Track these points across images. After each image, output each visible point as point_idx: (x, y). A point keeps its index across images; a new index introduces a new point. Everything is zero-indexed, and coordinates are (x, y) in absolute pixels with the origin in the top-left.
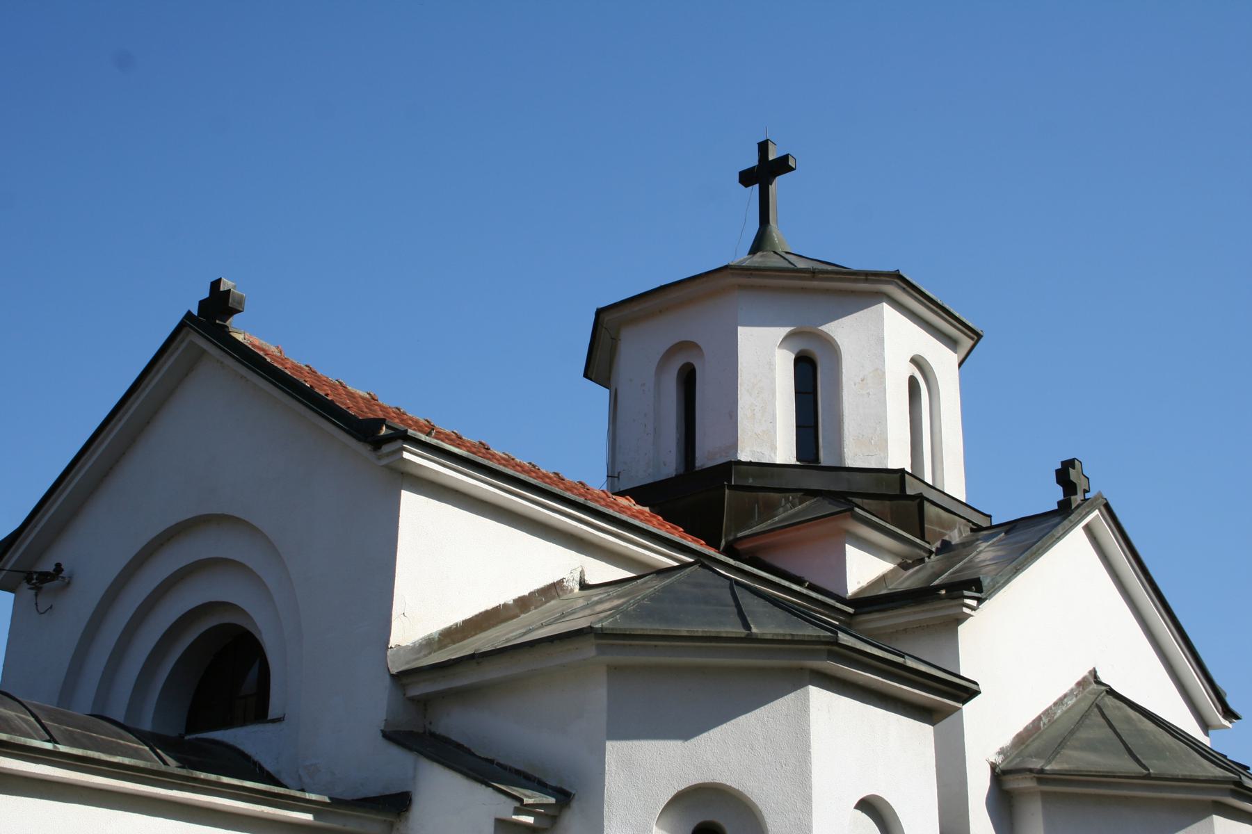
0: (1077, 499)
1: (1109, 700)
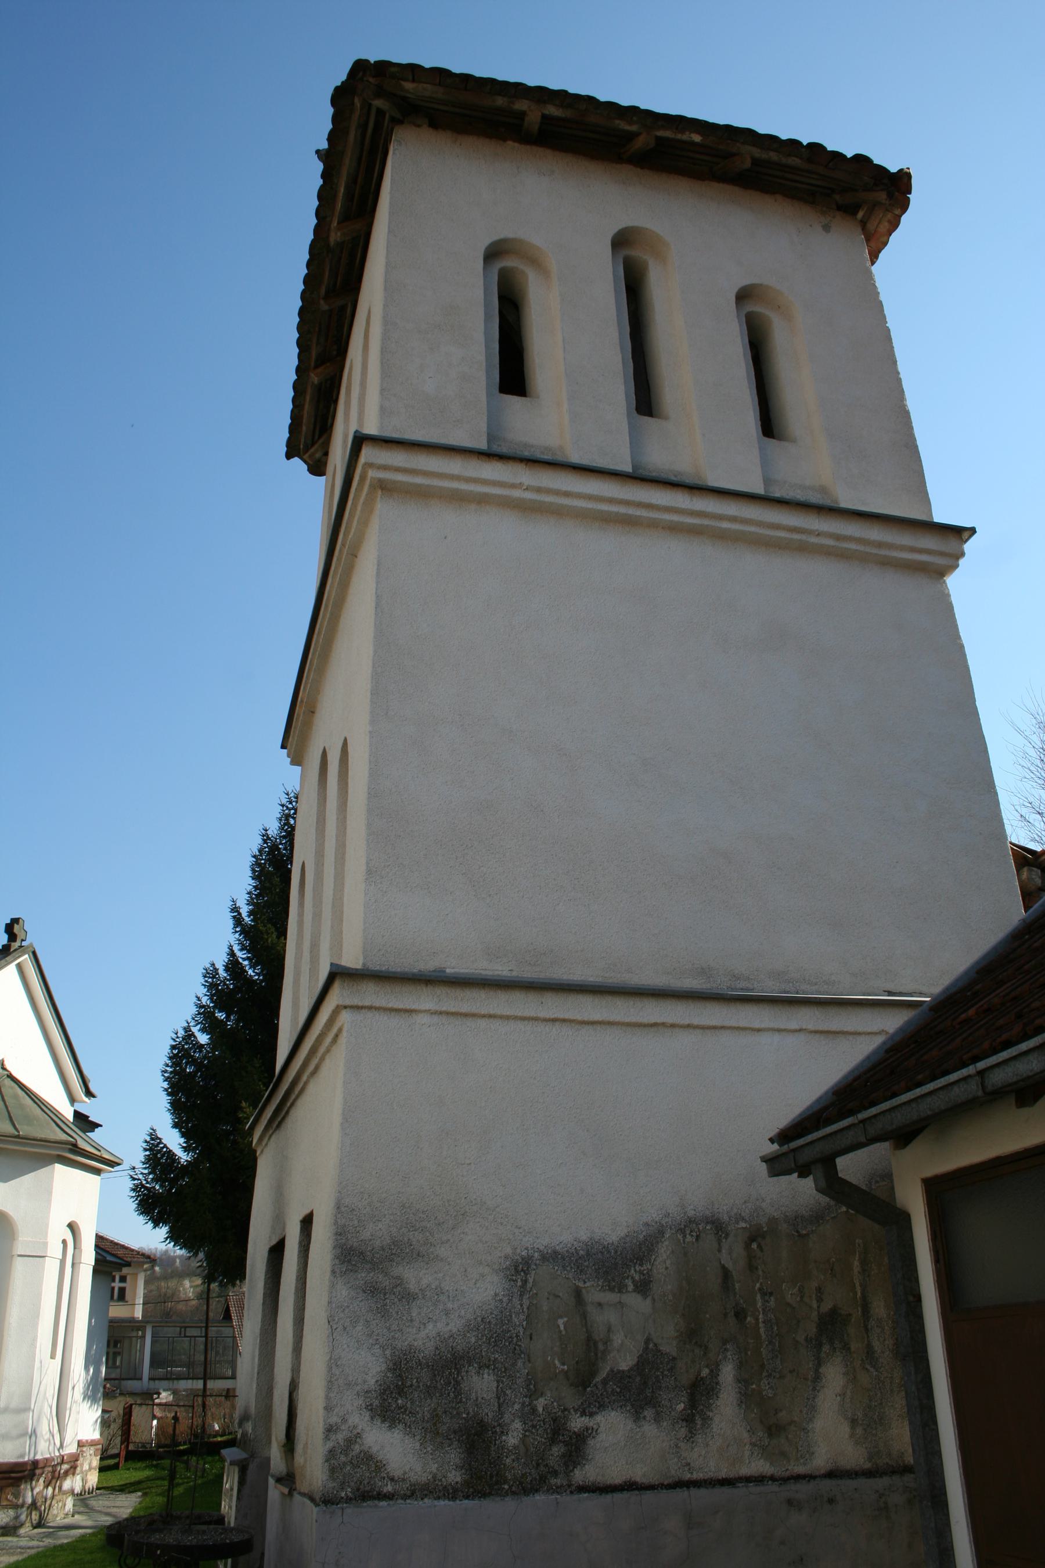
0: (15, 945)
1: (8, 1082)
